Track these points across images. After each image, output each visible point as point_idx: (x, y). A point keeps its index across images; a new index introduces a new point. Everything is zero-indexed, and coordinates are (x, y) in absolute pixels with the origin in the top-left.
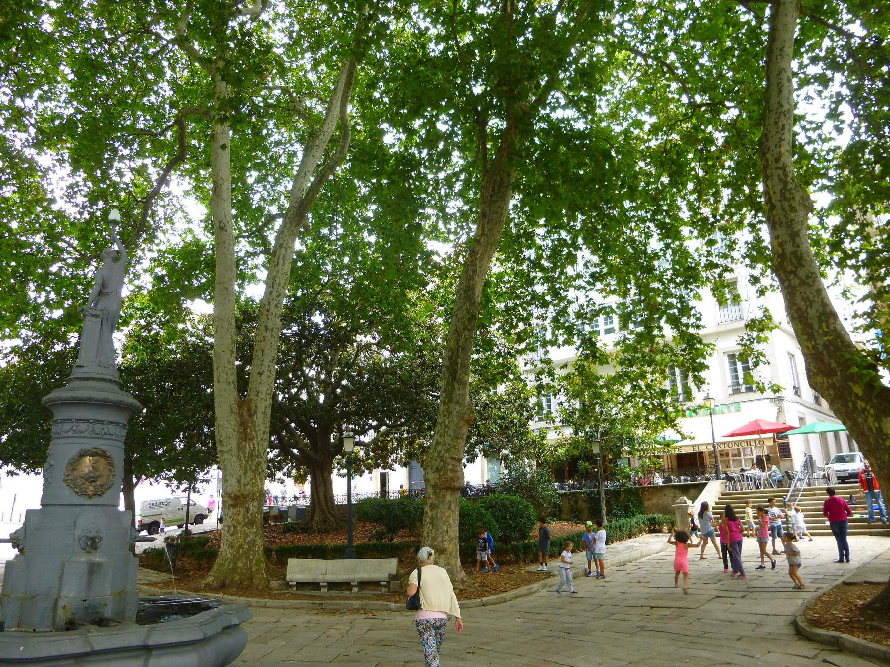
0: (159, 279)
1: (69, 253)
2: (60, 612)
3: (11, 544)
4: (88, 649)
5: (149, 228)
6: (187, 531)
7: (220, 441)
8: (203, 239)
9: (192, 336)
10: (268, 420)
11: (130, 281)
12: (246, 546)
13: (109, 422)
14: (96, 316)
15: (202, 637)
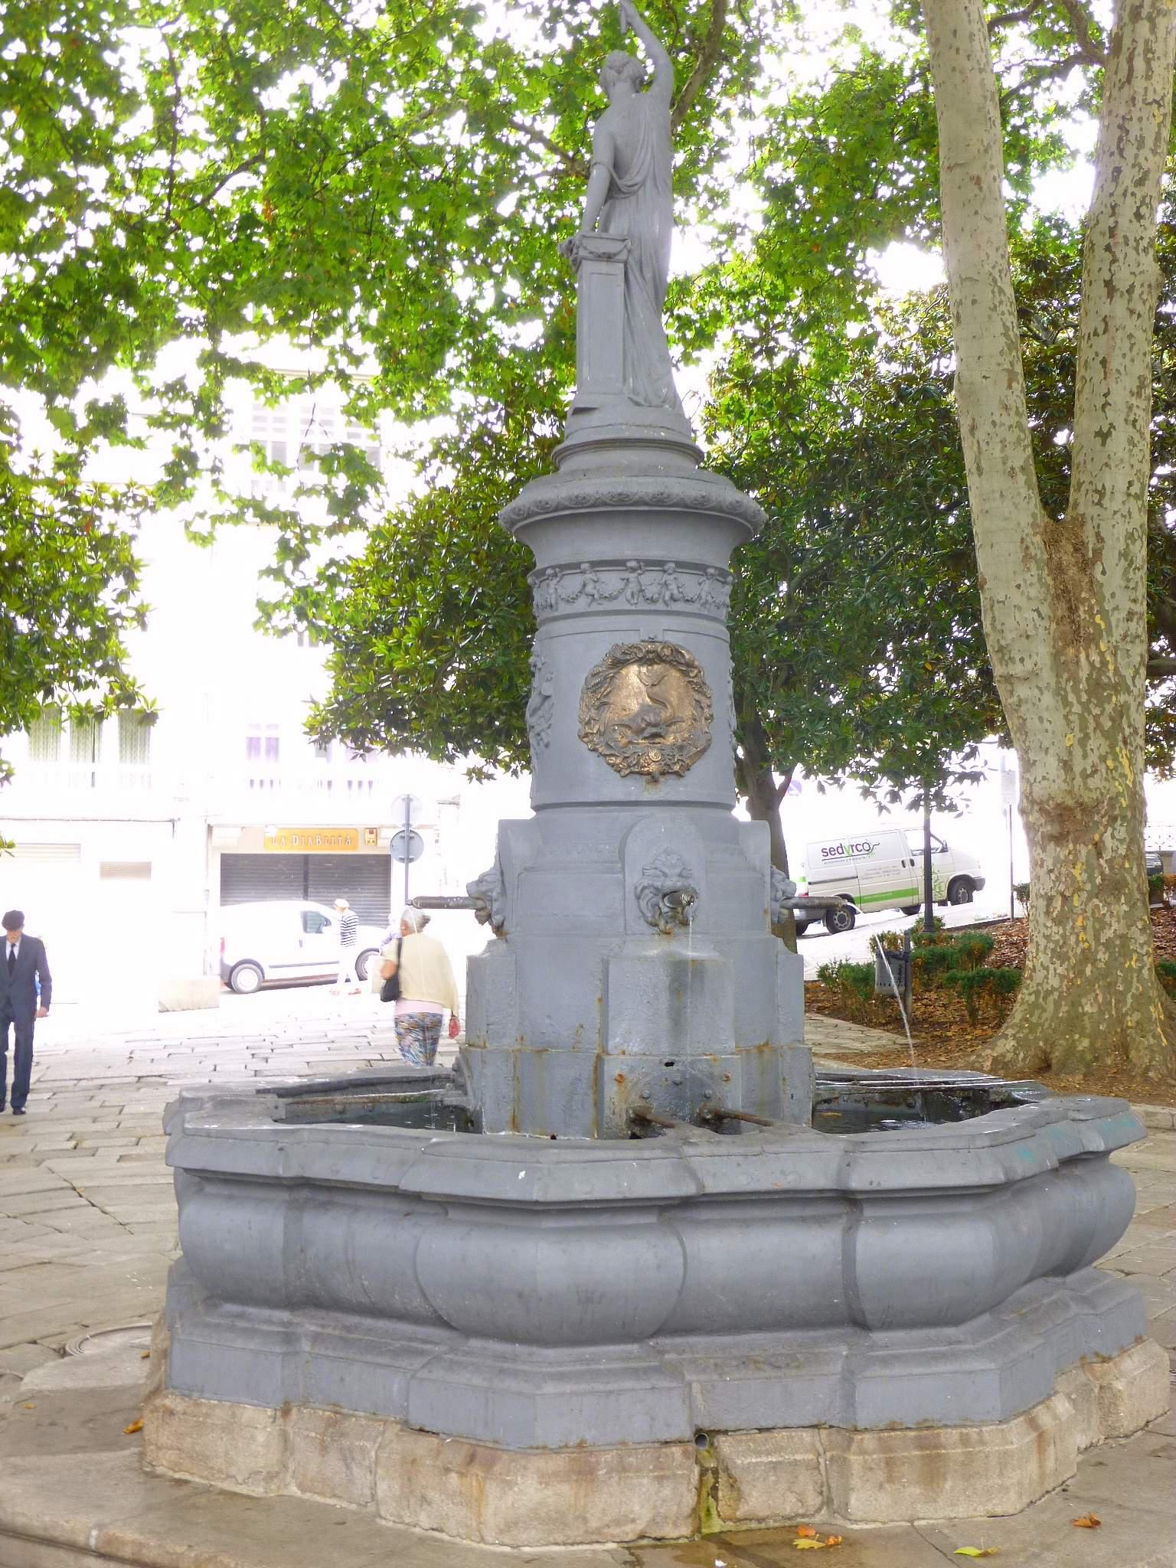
0: (780, 194)
1: (535, 158)
2: (611, 1091)
3: (471, 913)
4: (689, 1189)
5: (735, 46)
6: (931, 923)
7: (1001, 649)
8: (892, 54)
9: (890, 359)
10: (1140, 577)
11: (704, 213)
12: (1103, 956)
13: (680, 564)
14: (609, 257)
15: (1001, 1178)
